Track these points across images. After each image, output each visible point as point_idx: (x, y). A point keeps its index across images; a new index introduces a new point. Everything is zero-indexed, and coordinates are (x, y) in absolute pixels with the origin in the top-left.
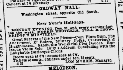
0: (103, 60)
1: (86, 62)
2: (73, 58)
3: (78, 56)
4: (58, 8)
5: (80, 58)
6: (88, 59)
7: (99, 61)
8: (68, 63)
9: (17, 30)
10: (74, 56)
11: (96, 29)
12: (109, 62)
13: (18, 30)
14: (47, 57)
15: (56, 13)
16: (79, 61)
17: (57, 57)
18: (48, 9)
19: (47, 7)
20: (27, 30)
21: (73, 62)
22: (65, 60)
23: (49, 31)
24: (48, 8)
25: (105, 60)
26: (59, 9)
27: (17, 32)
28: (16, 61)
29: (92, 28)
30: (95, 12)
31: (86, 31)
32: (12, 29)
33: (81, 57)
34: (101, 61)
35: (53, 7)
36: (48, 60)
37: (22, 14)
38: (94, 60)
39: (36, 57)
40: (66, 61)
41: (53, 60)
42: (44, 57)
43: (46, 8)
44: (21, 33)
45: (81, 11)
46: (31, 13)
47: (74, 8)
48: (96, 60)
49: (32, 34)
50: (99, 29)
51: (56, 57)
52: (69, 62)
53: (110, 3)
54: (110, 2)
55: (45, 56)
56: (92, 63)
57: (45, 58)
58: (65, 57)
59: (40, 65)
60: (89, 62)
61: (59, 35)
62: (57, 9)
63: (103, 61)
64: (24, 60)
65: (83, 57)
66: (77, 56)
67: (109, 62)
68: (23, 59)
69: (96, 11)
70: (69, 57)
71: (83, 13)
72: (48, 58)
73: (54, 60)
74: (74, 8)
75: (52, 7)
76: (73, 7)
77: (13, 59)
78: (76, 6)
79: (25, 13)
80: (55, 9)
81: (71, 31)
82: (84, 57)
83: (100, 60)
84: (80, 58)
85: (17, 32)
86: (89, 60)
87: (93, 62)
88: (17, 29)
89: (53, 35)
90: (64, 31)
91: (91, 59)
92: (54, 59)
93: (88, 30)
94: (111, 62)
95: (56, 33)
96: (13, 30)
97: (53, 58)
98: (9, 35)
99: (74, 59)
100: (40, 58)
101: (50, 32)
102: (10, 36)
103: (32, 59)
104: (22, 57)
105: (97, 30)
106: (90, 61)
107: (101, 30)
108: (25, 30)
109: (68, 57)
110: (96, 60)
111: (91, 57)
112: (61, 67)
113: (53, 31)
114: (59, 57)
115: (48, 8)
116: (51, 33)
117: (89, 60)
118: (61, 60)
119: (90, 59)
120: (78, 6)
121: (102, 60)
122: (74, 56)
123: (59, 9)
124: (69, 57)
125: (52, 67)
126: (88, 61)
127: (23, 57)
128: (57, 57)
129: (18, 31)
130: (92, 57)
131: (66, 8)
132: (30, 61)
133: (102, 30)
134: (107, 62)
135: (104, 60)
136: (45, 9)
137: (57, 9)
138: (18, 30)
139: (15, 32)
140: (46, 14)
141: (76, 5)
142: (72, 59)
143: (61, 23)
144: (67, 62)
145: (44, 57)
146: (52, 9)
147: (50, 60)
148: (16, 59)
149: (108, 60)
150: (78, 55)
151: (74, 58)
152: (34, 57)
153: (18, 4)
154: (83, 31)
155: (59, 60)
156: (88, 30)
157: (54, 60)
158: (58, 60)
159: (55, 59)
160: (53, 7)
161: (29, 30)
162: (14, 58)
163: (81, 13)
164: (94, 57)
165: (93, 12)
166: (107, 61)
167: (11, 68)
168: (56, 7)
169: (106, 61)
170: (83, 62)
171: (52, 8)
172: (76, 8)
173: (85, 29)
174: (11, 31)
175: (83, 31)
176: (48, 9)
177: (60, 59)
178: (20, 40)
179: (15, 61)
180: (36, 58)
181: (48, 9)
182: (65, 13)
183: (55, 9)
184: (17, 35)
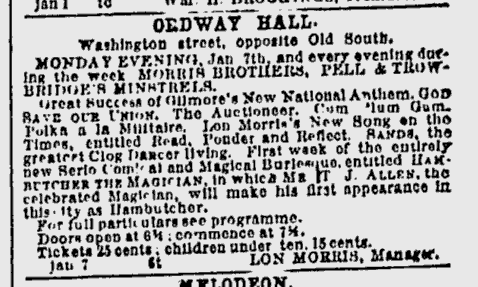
1: (334, 260)
2: (282, 243)
4: (228, 24)
5: (308, 243)
7: (385, 255)
8: (258, 263)
9: (56, 63)
10: (283, 235)
11: (375, 65)
14: (174, 240)
15: (221, 44)
17: (216, 242)
18: (186, 26)
21: (280, 259)
22: (250, 253)
23: (187, 74)
24: (186, 22)
25: (412, 254)
27: (56, 75)
29: (363, 57)
30: (379, 39)
32: (38, 60)
33: (315, 239)
34: (393, 255)
35: (211, 19)
39: (129, 238)
40: (253, 256)
41: (199, 252)
42: (161, 239)
44: (75, 76)
45: (322, 35)
46: (118, 41)
47: (295, 24)
49: (117, 85)
50: (388, 64)
51: (209, 242)
52: (266, 259)
53: (448, 265)
54: (446, 262)
55: (165, 237)
56: (358, 264)
57: (165, 242)
58: (248, 241)
59: (155, 270)
60: (345, 260)
62: (224, 29)
63: (404, 256)
64: (82, 249)
65: (322, 240)
66: (296, 235)
67: (427, 262)
69: (382, 35)
70: (265, 241)
71: (331, 43)
72: (180, 243)
74: (295, 24)
75: (204, 19)
76: (292, 22)
78: (304, 17)
79: (92, 41)
80: (217, 29)
81: (274, 75)
82: (327, 242)
83: (389, 253)
84: (308, 243)
85: (56, 75)
88: (58, 59)
90: (249, 72)
91: (355, 248)
92: (202, 249)
93: (343, 68)
94: (434, 262)
95: (215, 83)
96: (41, 64)
98: (26, 87)
99: (283, 249)
100: (146, 244)
101: (191, 77)
102: (30, 93)
103: (113, 246)
105: (381, 70)
106: (349, 257)
107: (397, 72)
108: (89, 62)
109: (259, 240)
110: (374, 251)
112: (229, 280)
114: (222, 241)
115: (186, 22)
116: (191, 82)
117: (345, 252)
118: (233, 251)
121: (396, 253)
122: (283, 235)
124: (265, 241)
125: (190, 282)
126: (342, 257)
127: (78, 239)
128: (216, 242)
130: (357, 240)
131: (261, 23)
133: (401, 68)
135: (408, 253)
137: (224, 29)
139: (49, 73)
141: (305, 13)
142: (275, 248)
143: (235, 99)
144: (256, 262)
145: (161, 239)
146: (207, 29)
150: (299, 233)
151: (285, 246)
152: (124, 237)
153: (64, 197)
154: (324, 74)
155: (224, 252)
156: (343, 68)
157: (205, 252)
160: (211, 19)
161: (106, 66)
162: (41, 243)
163: (322, 43)
164: (365, 241)
166: (420, 256)
167: (28, 19)
168: (220, 18)
169: (416, 258)
170: (323, 261)
171: (203, 24)
172: (301, 25)
174: (32, 69)
175: (324, 74)
177: (228, 249)
179: (46, 253)
180: (129, 245)
181: (186, 26)
183: (217, 29)
184: (57, 86)
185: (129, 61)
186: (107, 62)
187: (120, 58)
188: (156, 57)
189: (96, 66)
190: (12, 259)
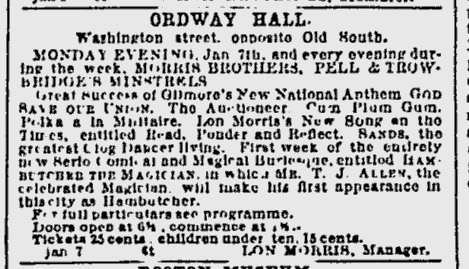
0: (391, 249)
2: (274, 236)
3: (290, 232)
5: (299, 236)
6: (333, 245)
7: (376, 250)
12: (418, 256)
13: (60, 55)
16: (297, 250)
18: (183, 21)
19: (180, 14)
20: (93, 59)
22: (242, 244)
24: (183, 17)
25: (403, 250)
26: (230, 25)
28: (45, 243)
31: (328, 72)
33: (306, 235)
36: (173, 242)
37: (78, 34)
38: (357, 249)
39: (122, 228)
40: (245, 247)
41: (192, 242)
43: (176, 19)
47: (289, 22)
48: (365, 247)
50: (382, 63)
57: (158, 233)
60: (336, 254)
61: (216, 82)
62: (219, 25)
63: (394, 251)
68: (72, 235)
69: (377, 34)
70: (257, 234)
73: (197, 242)
77: (32, 234)
78: (298, 15)
79: (89, 34)
80: (212, 25)
82: (318, 237)
84: (299, 236)
86: (336, 247)
87: (353, 255)
89: (196, 85)
92: (195, 240)
95: (210, 78)
97: (192, 235)
99: (275, 242)
100: (140, 234)
104: (67, 229)
105: (374, 70)
108: (86, 55)
109: (251, 234)
110: (365, 247)
111: (345, 236)
113: (197, 68)
115: (183, 17)
117: (336, 247)
119: (340, 245)
120: (306, 15)
121: (387, 249)
123: (230, 25)
129: (58, 60)
130: (349, 236)
132: (98, 245)
134: (407, 254)
136: (172, 24)
137: (219, 25)
138: (60, 55)
140: (174, 38)
142: (267, 241)
143: (229, 95)
147: (178, 242)
148: (44, 233)
149: (415, 251)
150: (290, 229)
151: (277, 239)
155: (216, 242)
156: (337, 67)
157: (197, 242)
158: (212, 242)
159: (200, 240)
162: (35, 230)
165: (367, 38)
166: (410, 252)
167: (26, 11)
169: (407, 254)
172: (295, 22)
173: (326, 62)
175: (318, 72)
176: (185, 24)
177: (220, 240)
178: (65, 192)
180: (123, 235)
181: (183, 21)
182: (254, 38)
183: (212, 25)
185: (125, 54)
186: (231, 20)
187: (117, 51)
188: (153, 52)
189: (93, 59)
190: (7, 96)
